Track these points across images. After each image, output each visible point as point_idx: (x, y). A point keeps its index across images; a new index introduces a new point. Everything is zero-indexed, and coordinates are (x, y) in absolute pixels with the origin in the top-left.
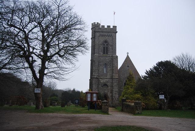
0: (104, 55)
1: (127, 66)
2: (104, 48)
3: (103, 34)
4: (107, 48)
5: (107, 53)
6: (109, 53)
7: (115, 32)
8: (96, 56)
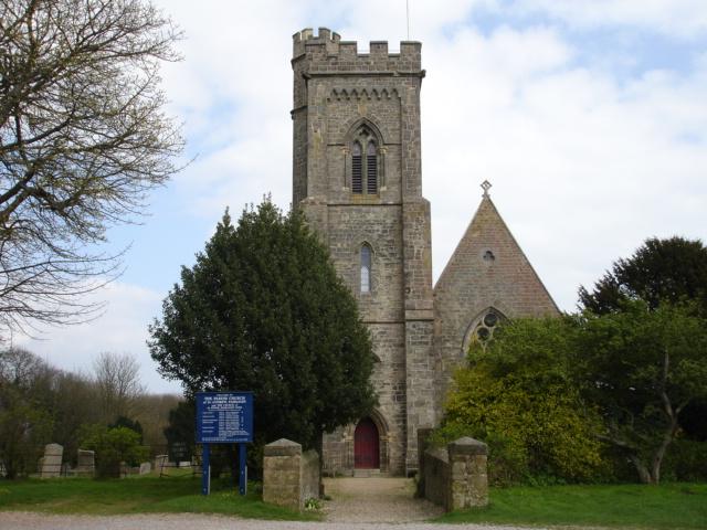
0: (358, 198)
1: (483, 252)
2: (357, 160)
3: (349, 85)
4: (372, 160)
5: (373, 189)
6: (383, 189)
7: (414, 75)
8: (313, 203)
